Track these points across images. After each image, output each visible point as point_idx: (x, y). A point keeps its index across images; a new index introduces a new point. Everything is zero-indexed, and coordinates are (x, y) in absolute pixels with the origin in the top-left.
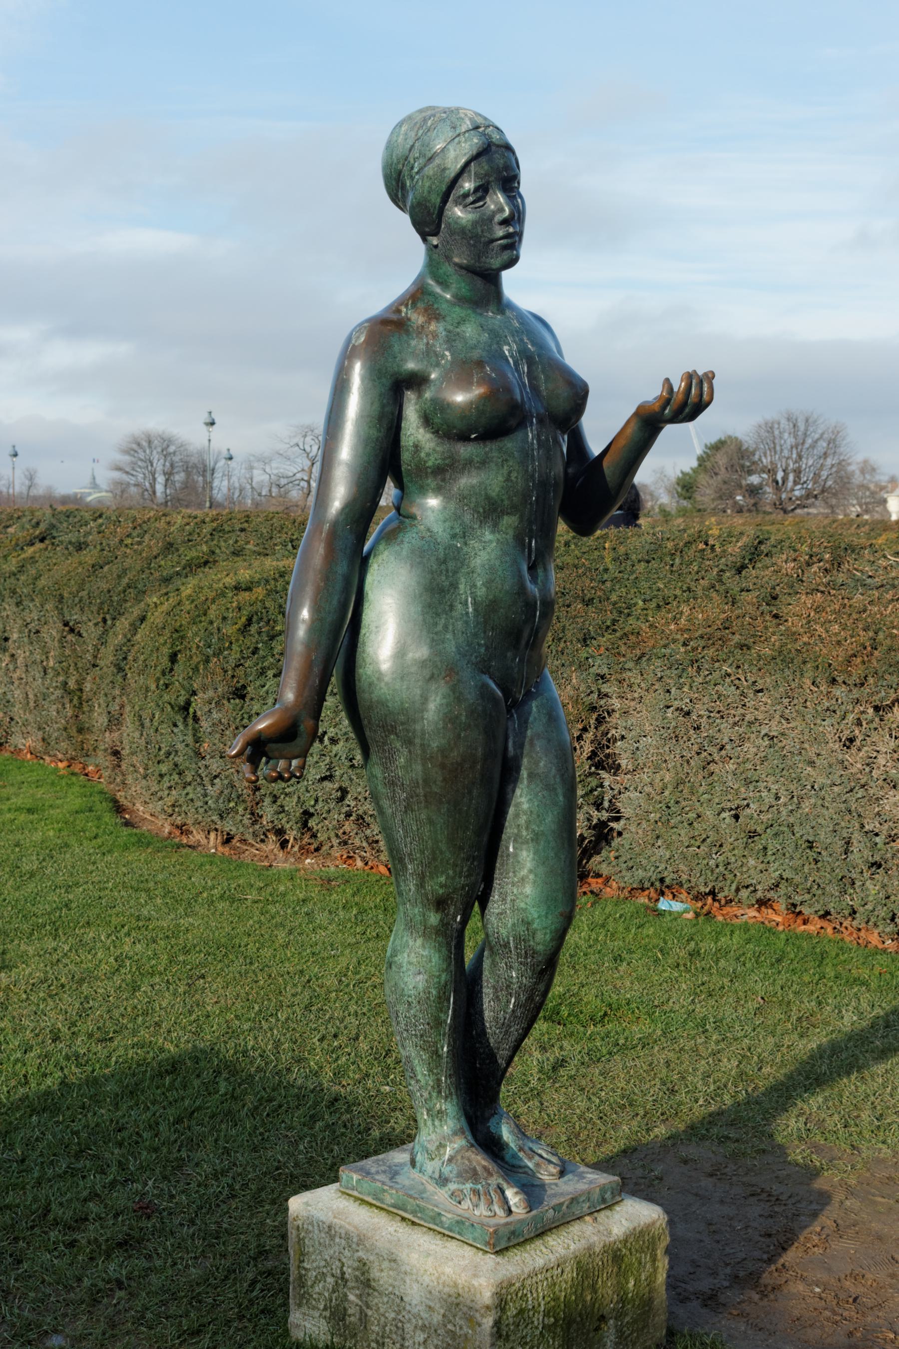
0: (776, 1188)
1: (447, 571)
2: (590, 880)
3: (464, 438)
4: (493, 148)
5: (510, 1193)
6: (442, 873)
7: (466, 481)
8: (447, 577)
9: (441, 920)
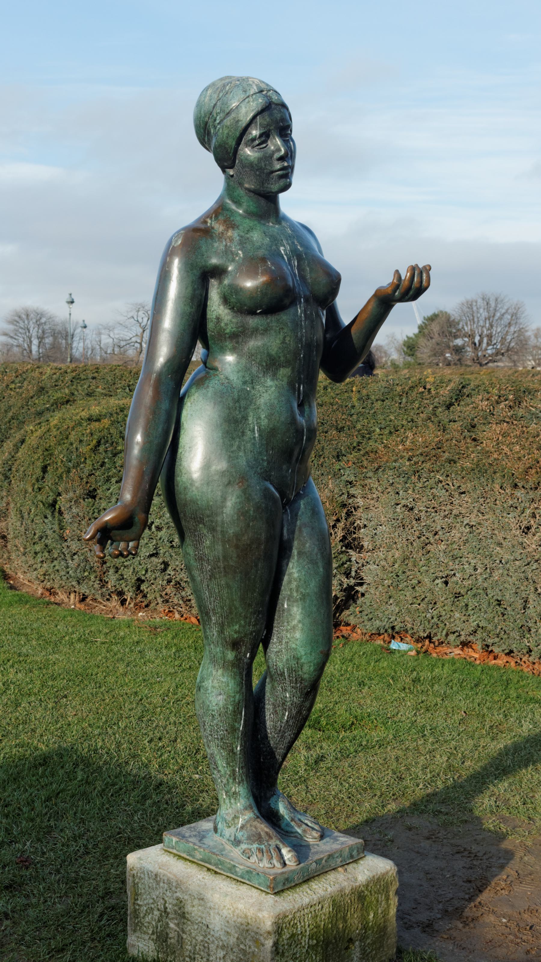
0: (475, 848)
1: (240, 408)
2: (342, 628)
3: (252, 312)
4: (273, 106)
5: (284, 851)
6: (236, 623)
7: (253, 344)
8: (240, 412)
9: (236, 657)
